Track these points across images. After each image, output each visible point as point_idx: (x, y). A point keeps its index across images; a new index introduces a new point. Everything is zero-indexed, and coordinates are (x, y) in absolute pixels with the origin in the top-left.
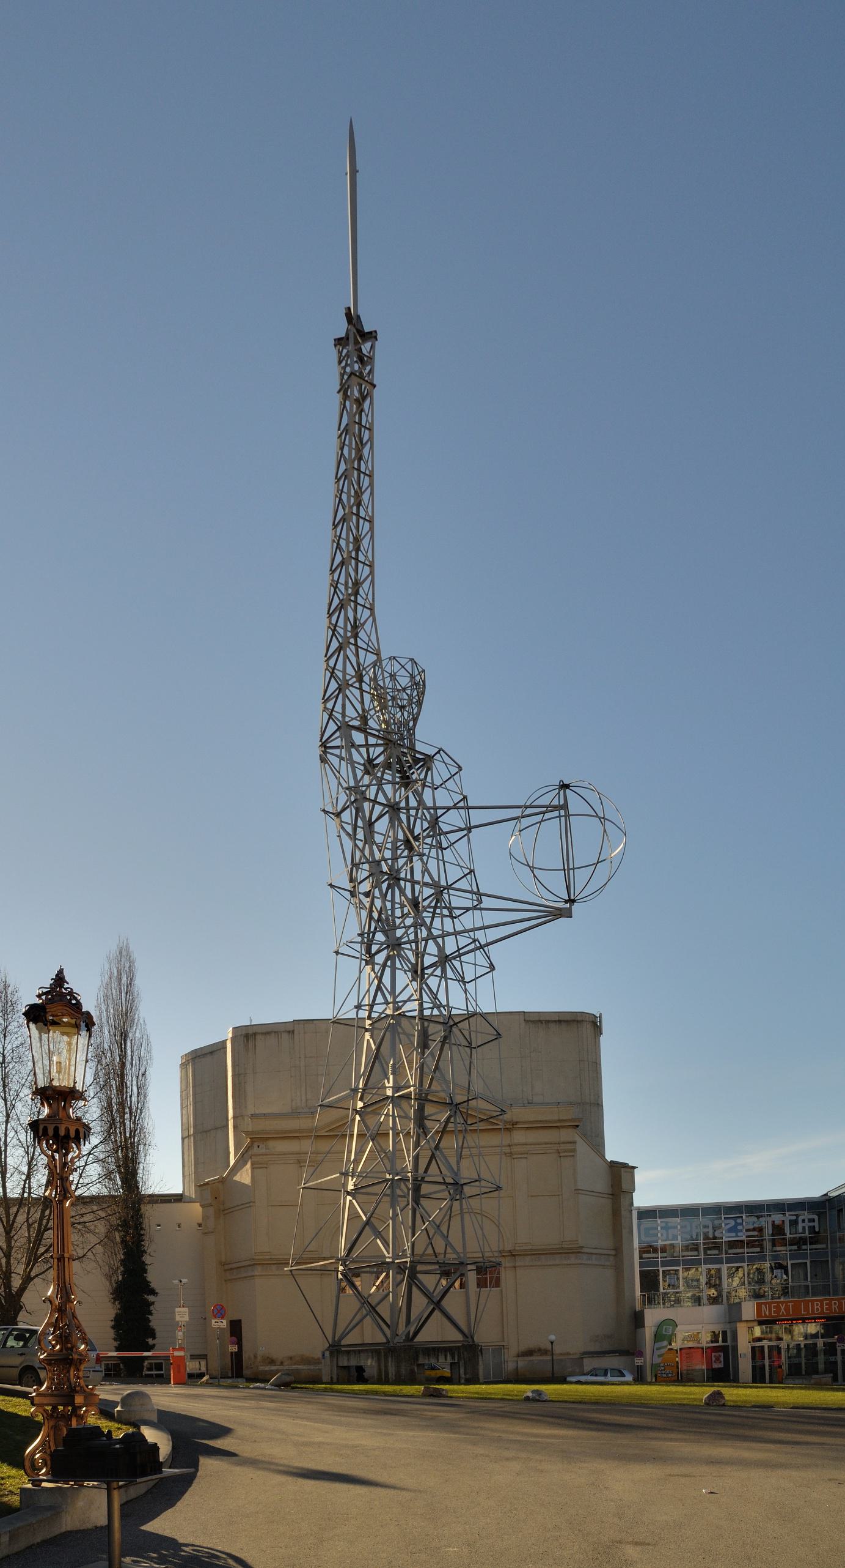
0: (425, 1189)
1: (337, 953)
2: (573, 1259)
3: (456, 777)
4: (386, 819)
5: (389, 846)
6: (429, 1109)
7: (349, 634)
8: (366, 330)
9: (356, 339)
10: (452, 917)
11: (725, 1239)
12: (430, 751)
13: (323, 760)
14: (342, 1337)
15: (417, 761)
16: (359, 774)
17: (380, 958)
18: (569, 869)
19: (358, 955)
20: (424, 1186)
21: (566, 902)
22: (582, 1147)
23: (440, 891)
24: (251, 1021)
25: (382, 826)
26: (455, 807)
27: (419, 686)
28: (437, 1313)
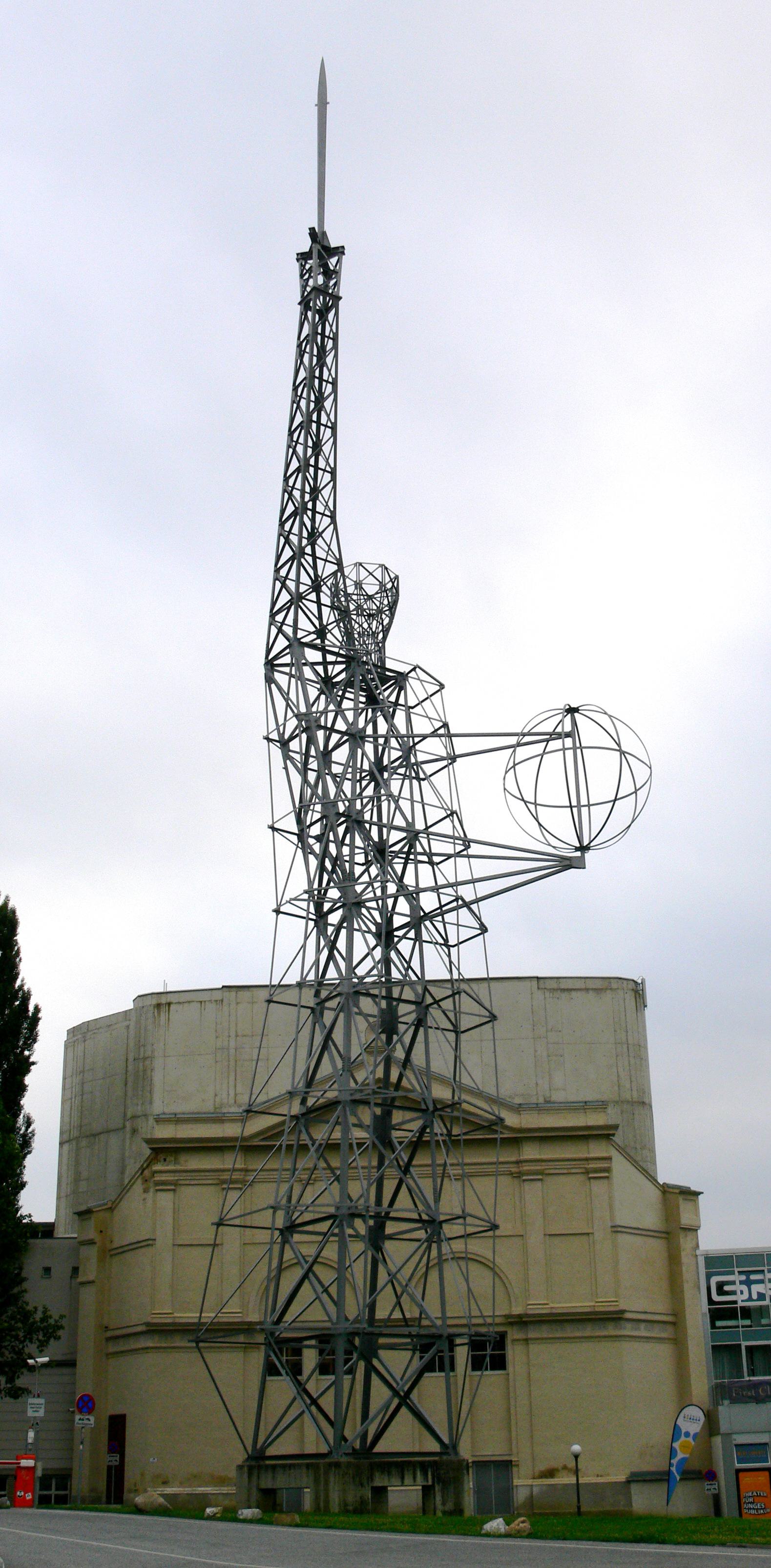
0: (391, 1228)
2: (611, 1330)
3: (436, 698)
4: (345, 749)
5: (349, 776)
6: (397, 1117)
7: (305, 542)
8: (333, 246)
9: (321, 255)
10: (431, 863)
12: (403, 668)
13: (270, 680)
14: (267, 1445)
15: (384, 680)
16: (313, 693)
17: (334, 918)
18: (579, 806)
19: (304, 914)
20: (389, 1224)
21: (577, 849)
22: (620, 1166)
23: (412, 835)
24: (165, 985)
25: (341, 755)
26: (434, 734)
27: (391, 592)
28: (404, 1410)
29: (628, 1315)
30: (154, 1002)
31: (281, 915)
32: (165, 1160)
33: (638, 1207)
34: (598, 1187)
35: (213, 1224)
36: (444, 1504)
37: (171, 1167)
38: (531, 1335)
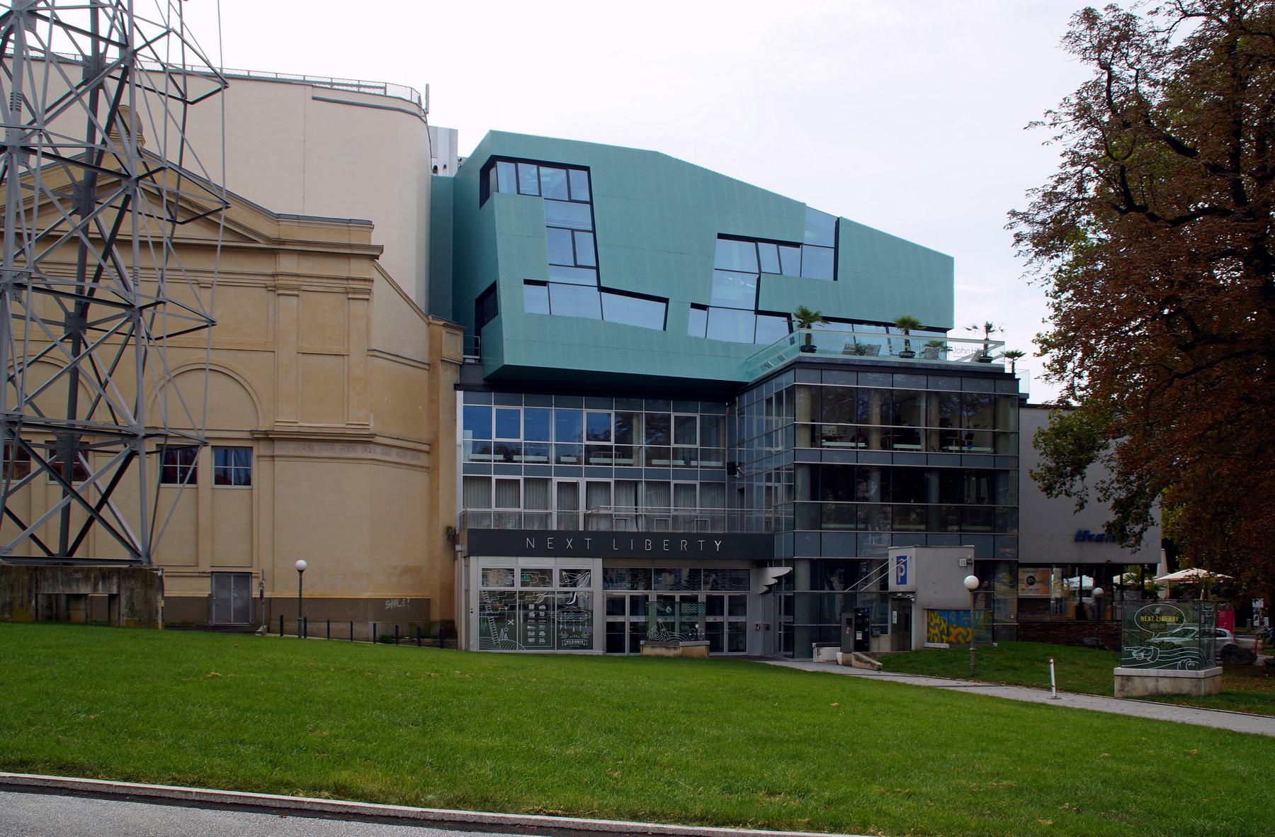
2: (359, 452)
34: (358, 307)
38: (277, 452)
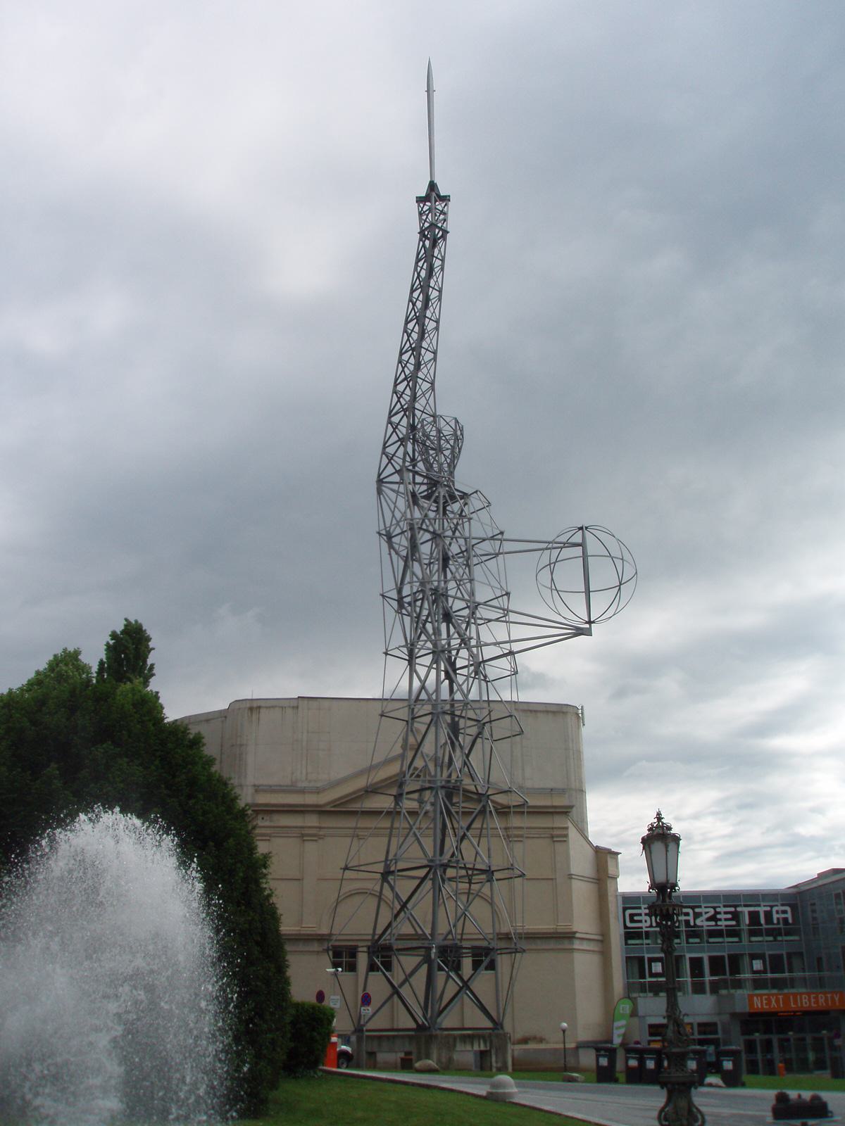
1: (386, 654)
8: (442, 195)
11: (705, 928)
13: (380, 492)
21: (587, 623)
29: (577, 935)
30: (248, 705)
31: (388, 656)
32: (263, 818)
33: (581, 864)
35: (341, 869)
36: (497, 1062)
37: (267, 824)
